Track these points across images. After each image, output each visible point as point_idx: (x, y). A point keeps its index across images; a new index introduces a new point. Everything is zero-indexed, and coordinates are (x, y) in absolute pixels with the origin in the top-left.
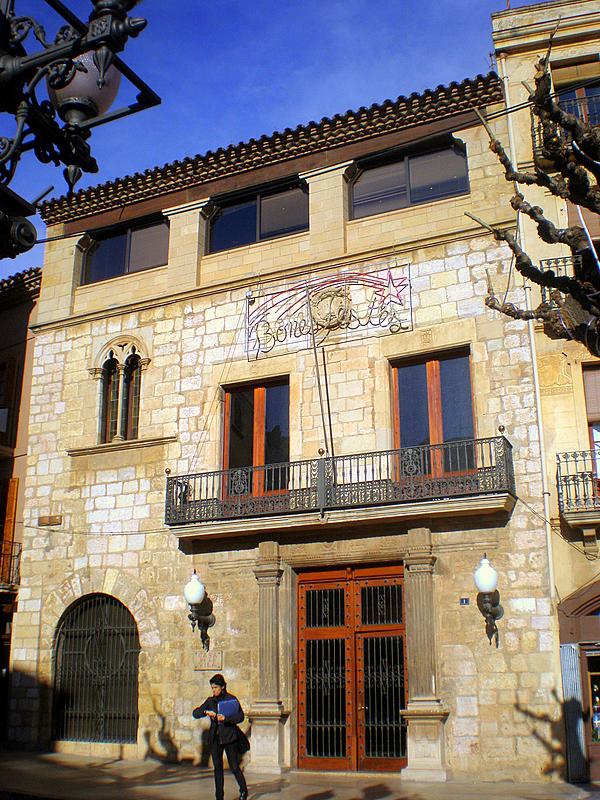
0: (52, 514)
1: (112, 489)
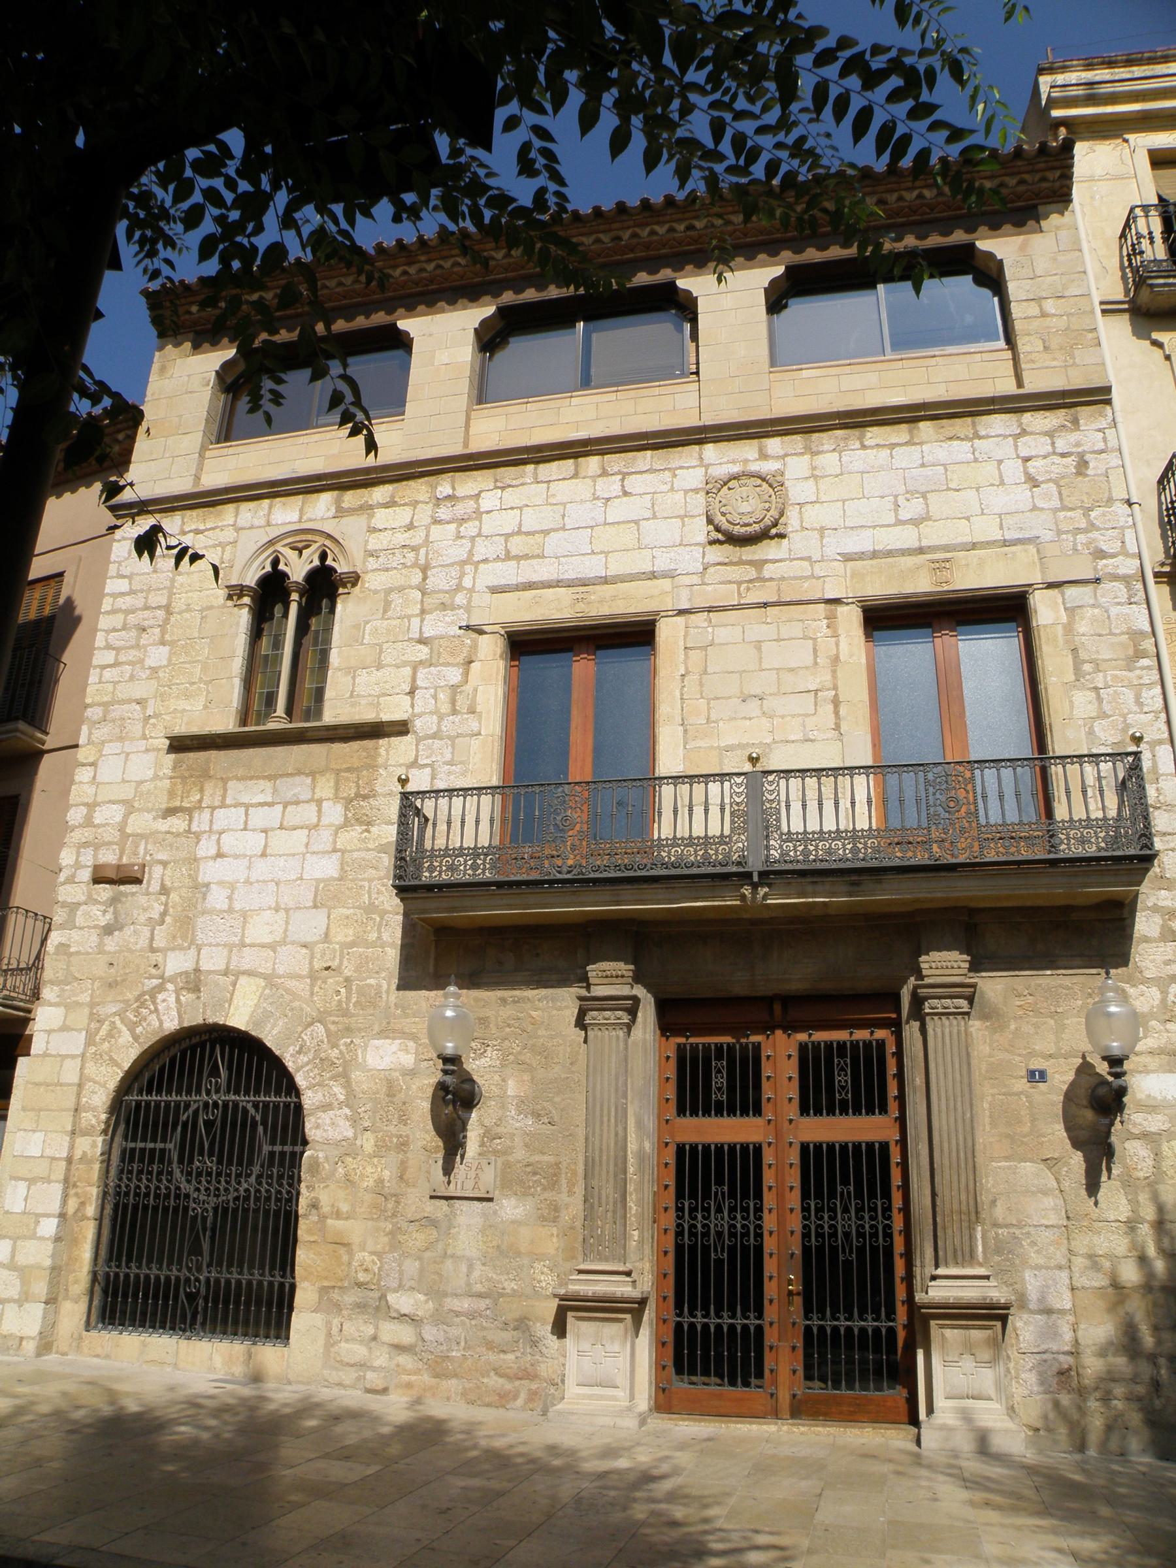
0: (125, 861)
1: (260, 817)
